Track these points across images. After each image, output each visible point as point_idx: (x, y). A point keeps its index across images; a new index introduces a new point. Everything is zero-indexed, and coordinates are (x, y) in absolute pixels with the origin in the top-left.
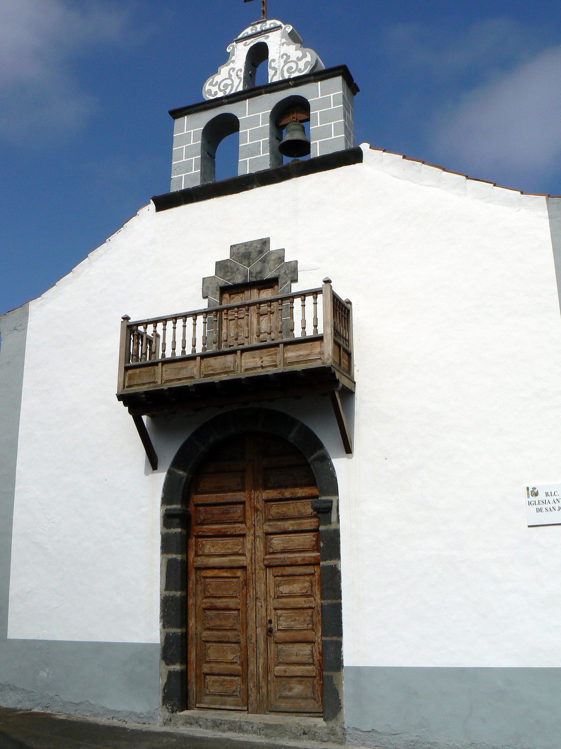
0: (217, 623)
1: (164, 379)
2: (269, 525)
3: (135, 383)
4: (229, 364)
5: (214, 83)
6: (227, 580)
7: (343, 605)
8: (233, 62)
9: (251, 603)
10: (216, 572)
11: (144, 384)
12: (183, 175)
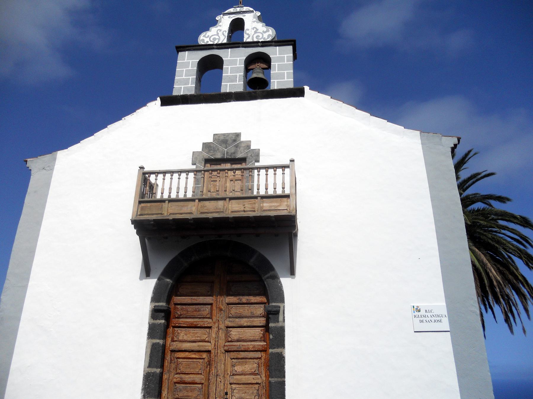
0: (185, 394)
1: (169, 212)
2: (229, 321)
3: (146, 212)
4: (220, 207)
5: (207, 36)
6: (195, 360)
7: (286, 383)
8: (220, 26)
9: (212, 378)
10: (187, 354)
11: (153, 214)
12: (183, 86)
